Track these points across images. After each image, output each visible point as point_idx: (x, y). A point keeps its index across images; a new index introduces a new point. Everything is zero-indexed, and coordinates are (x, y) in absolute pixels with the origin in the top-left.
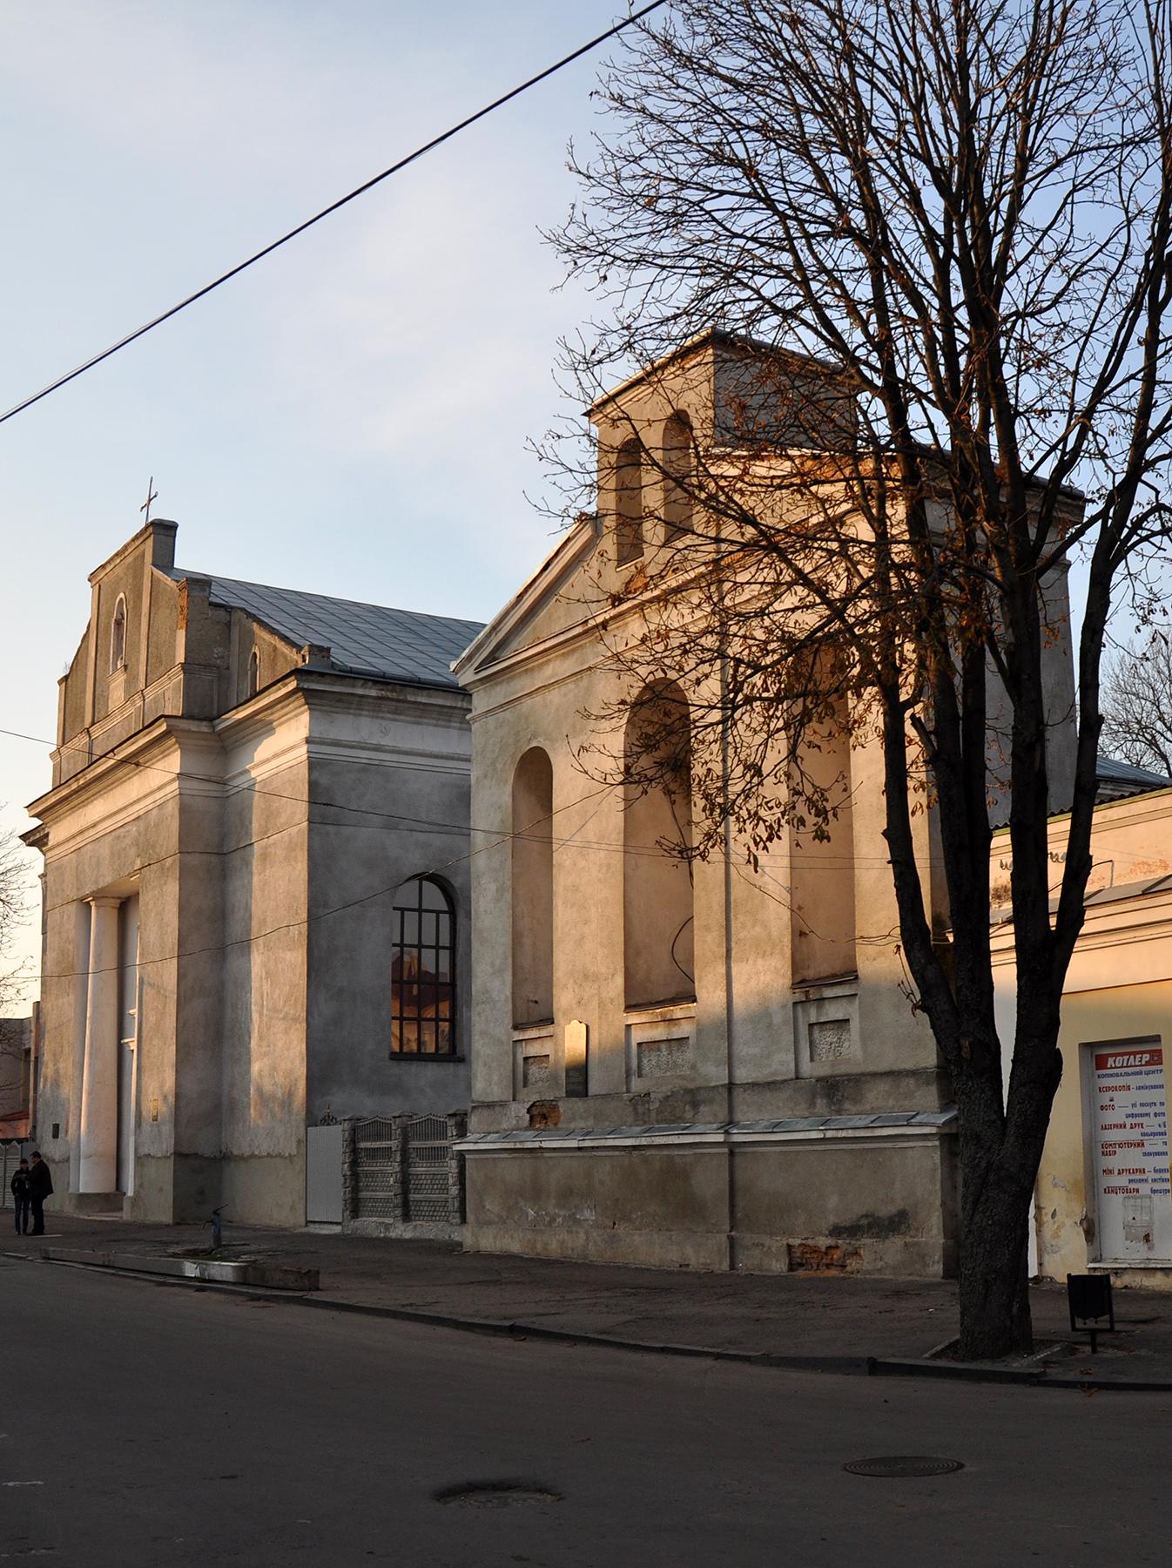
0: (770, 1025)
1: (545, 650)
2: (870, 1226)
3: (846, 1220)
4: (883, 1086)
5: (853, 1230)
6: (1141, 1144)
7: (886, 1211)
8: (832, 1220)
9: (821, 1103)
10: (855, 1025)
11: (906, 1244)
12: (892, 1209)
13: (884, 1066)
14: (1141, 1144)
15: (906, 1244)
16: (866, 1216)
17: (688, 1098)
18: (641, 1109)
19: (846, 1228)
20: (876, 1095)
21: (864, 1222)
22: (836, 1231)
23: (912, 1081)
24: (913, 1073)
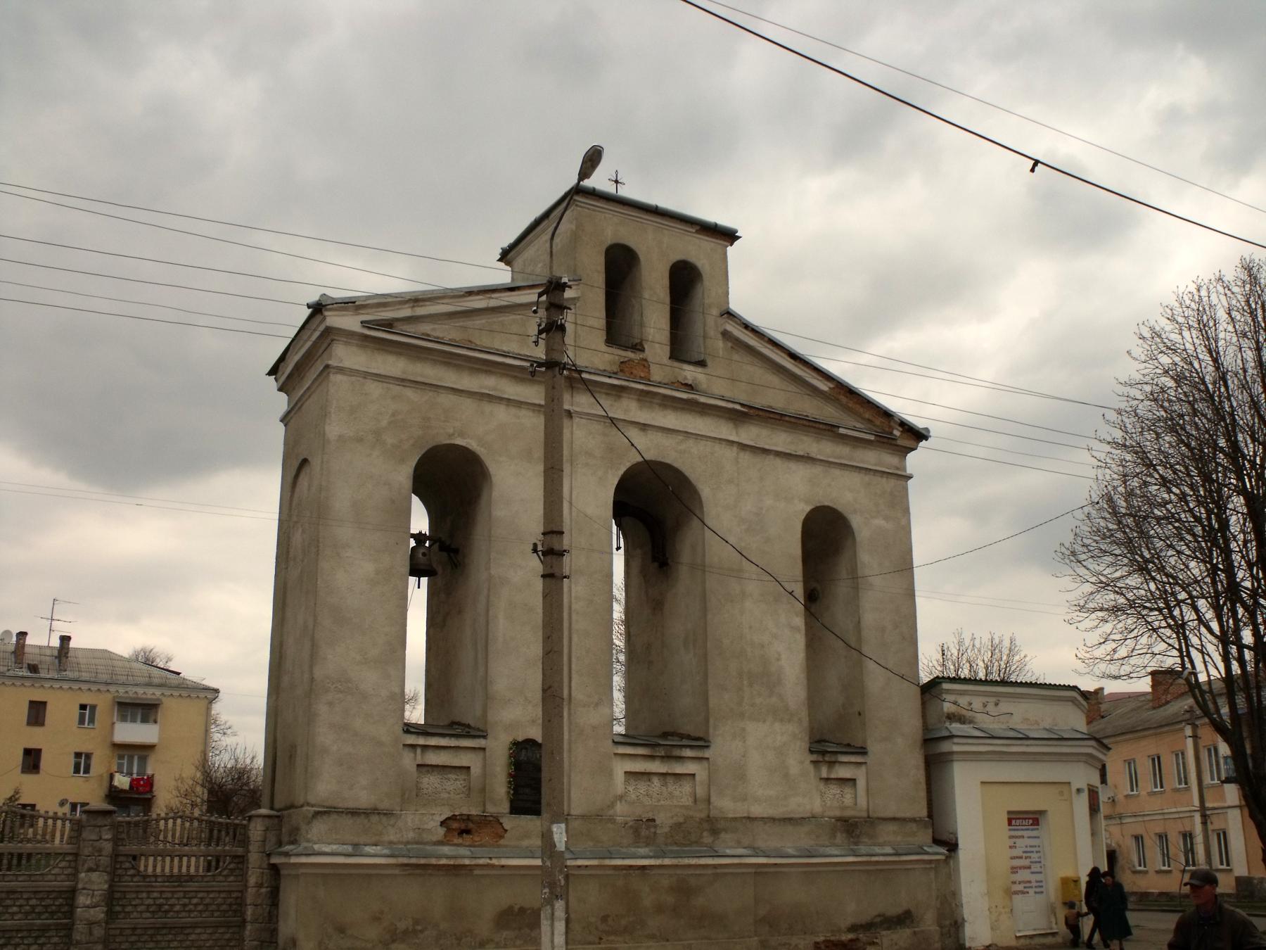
0: (786, 776)
1: (1024, 753)
2: (882, 923)
3: (865, 918)
4: (892, 827)
5: (869, 926)
6: (1029, 868)
7: (894, 911)
8: (850, 921)
9: (840, 838)
10: (861, 783)
11: (915, 933)
12: (899, 910)
13: (889, 814)
14: (1029, 868)
15: (915, 933)
16: (879, 916)
17: (706, 825)
18: (644, 832)
19: (861, 926)
20: (888, 833)
21: (878, 919)
22: (853, 928)
23: (914, 825)
24: (913, 820)
